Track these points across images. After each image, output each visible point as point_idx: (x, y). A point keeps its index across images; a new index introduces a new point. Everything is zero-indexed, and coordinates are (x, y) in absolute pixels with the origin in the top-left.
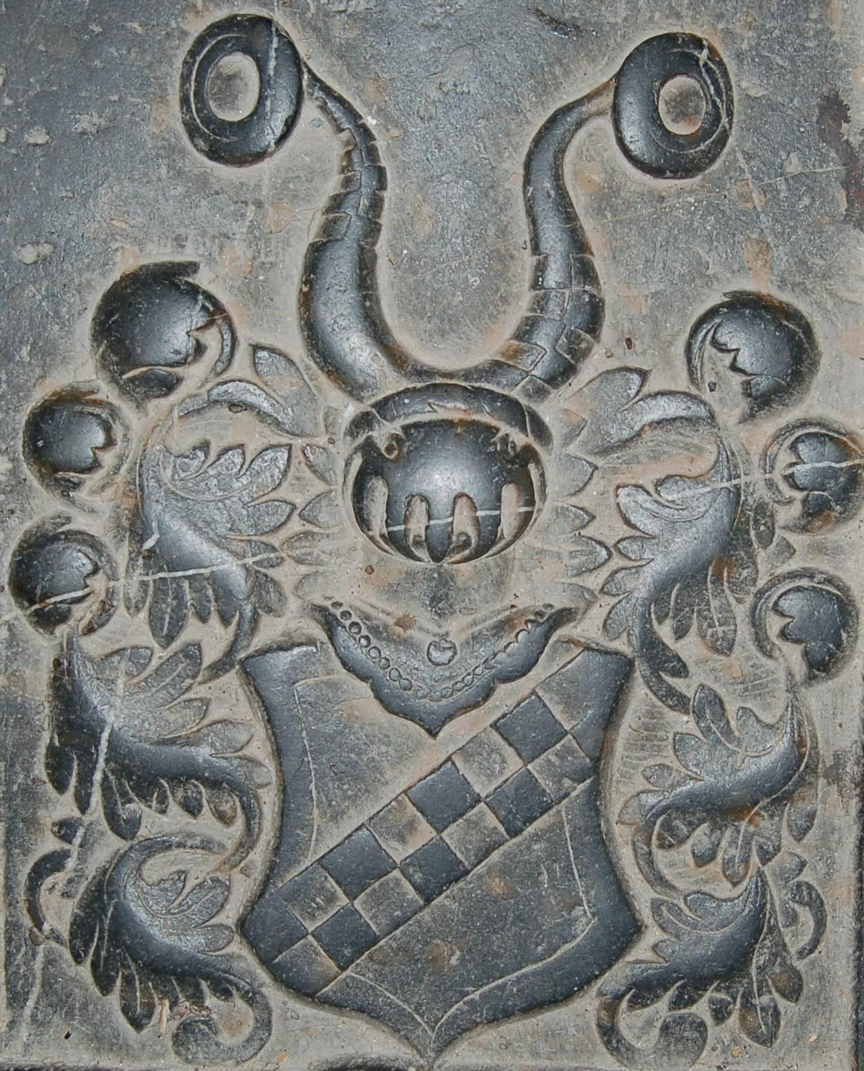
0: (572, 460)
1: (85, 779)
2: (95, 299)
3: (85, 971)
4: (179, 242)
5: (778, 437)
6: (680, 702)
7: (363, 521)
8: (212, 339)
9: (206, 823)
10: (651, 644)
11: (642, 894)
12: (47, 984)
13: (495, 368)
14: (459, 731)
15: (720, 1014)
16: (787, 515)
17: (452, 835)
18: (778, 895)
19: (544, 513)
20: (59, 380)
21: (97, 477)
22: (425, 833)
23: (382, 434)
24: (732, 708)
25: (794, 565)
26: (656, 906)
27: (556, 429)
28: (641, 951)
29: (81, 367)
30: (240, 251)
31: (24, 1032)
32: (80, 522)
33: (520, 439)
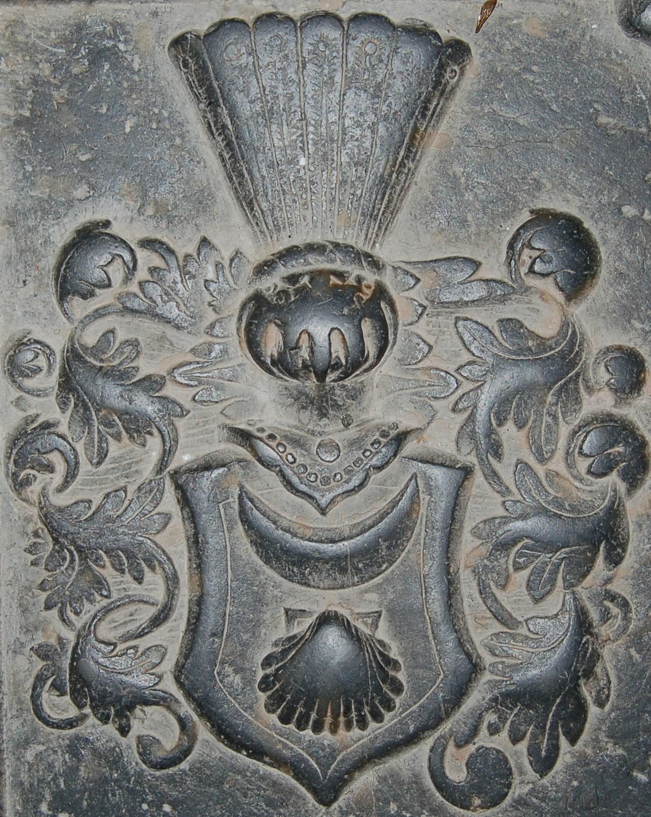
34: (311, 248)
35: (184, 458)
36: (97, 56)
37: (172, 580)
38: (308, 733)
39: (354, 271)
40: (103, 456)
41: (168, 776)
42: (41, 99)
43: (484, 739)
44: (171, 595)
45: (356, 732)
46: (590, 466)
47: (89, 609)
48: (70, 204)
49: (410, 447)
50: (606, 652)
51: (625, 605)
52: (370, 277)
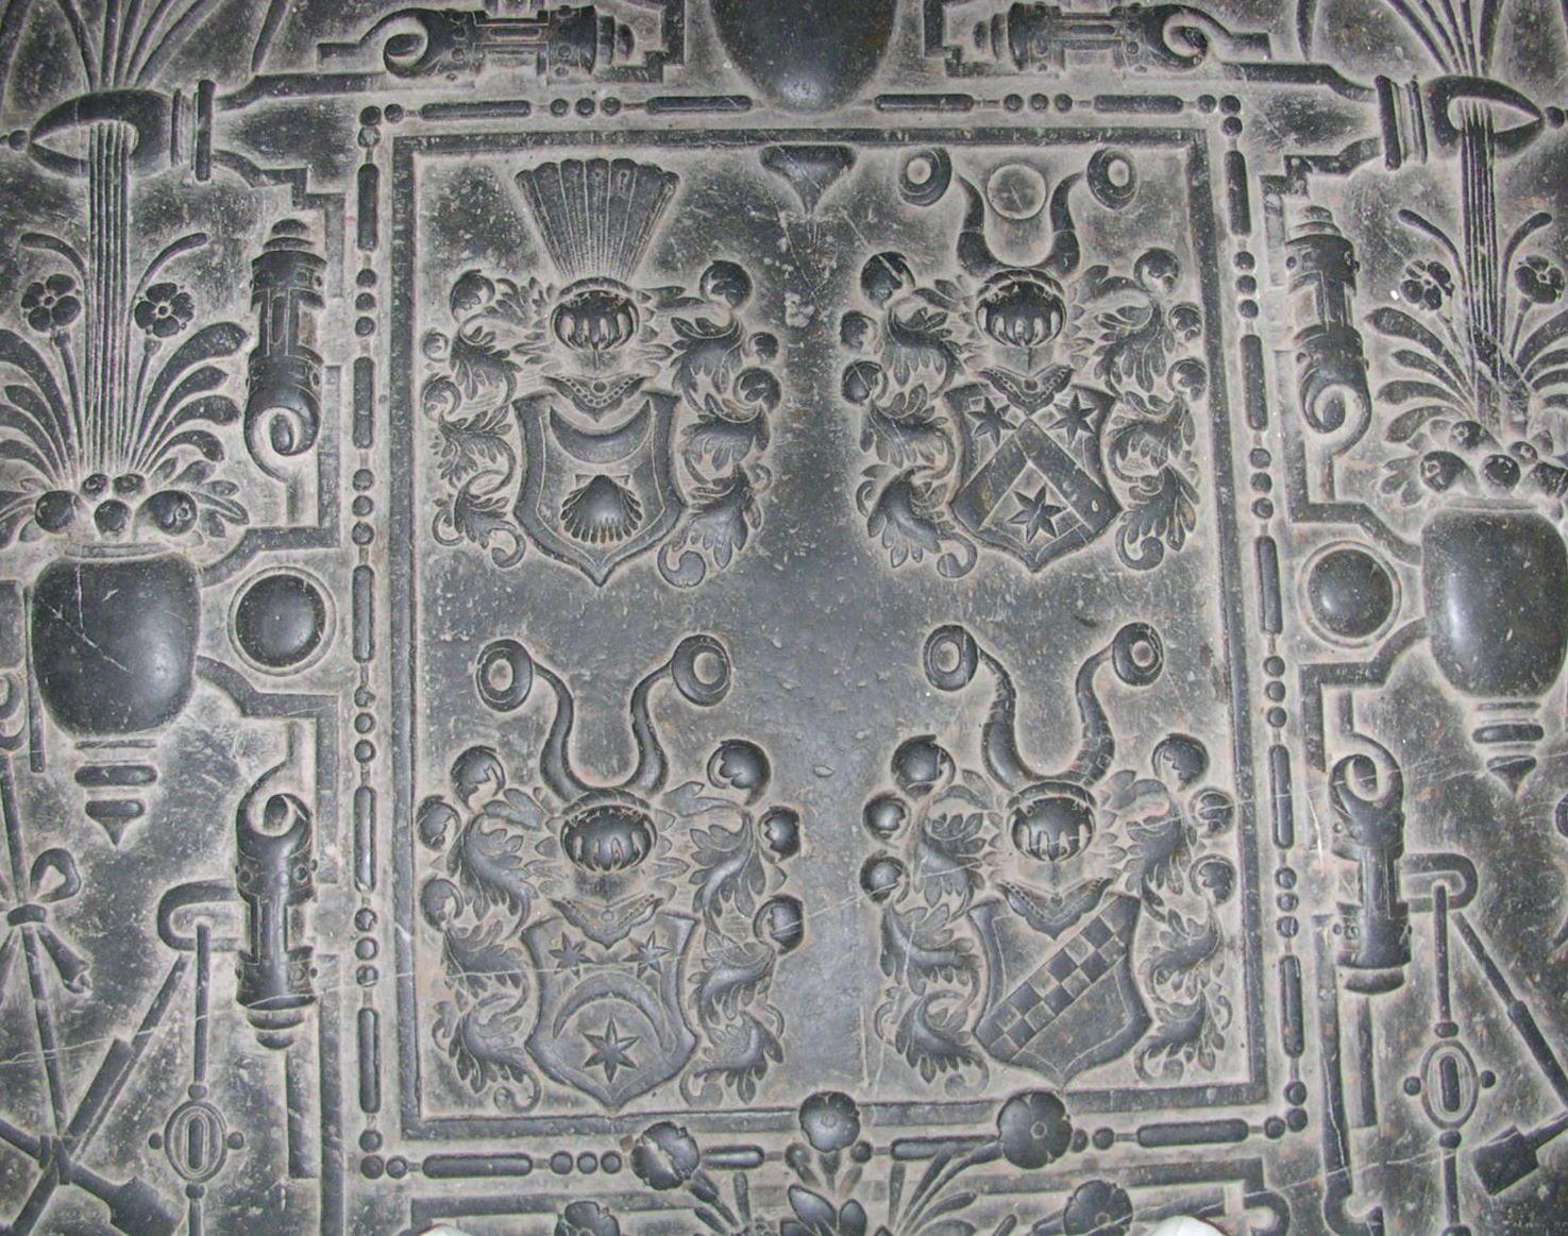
0: (1105, 813)
1: (900, 969)
2: (892, 753)
3: (903, 1057)
4: (927, 726)
5: (1195, 797)
6: (1161, 917)
7: (1018, 845)
8: (946, 767)
9: (955, 985)
10: (1147, 893)
11: (1151, 1006)
12: (886, 1067)
13: (1070, 774)
14: (1066, 936)
15: (1189, 1057)
16: (1202, 830)
17: (1066, 983)
18: (1210, 1002)
19: (1096, 838)
20: (877, 790)
21: (896, 834)
22: (1054, 984)
23: (1024, 806)
24: (1184, 919)
25: (1206, 853)
26: (1158, 1010)
27: (1098, 800)
28: (1153, 1031)
29: (888, 784)
30: (954, 728)
31: (876, 1087)
32: (891, 853)
33: (1084, 804)
34: (591, 280)
35: (517, 395)
36: (476, 185)
37: (512, 459)
38: (588, 543)
39: (614, 291)
40: (475, 391)
41: (517, 719)
42: (445, 207)
43: (689, 546)
44: (511, 468)
45: (616, 541)
46: (232, 520)
47: (466, 478)
48: (459, 262)
49: (646, 386)
50: (757, 498)
51: (768, 472)
52: (623, 295)
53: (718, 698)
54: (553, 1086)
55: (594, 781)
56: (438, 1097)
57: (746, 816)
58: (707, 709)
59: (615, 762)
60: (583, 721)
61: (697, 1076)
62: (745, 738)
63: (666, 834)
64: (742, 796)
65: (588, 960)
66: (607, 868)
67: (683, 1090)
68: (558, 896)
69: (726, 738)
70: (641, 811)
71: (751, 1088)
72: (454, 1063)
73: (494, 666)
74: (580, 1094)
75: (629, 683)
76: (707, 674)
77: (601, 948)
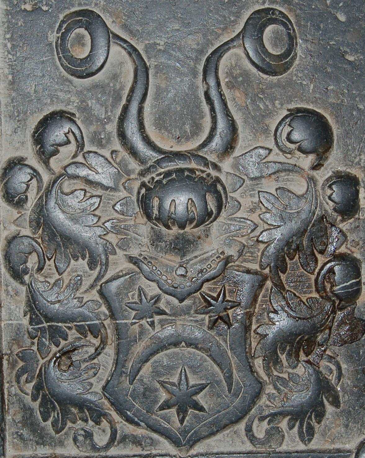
41: (95, 86)
53: (286, 67)
54: (130, 429)
55: (166, 145)
56: (21, 437)
57: (312, 180)
58: (275, 78)
59: (187, 128)
60: (158, 88)
61: (262, 419)
62: (310, 107)
63: (236, 195)
64: (307, 161)
65: (163, 313)
66: (182, 227)
67: (249, 429)
68: (134, 252)
69: (293, 106)
70: (214, 173)
71: (311, 432)
72: (36, 405)
73: (72, 35)
74: (155, 436)
75: (201, 52)
76: (275, 45)
77: (175, 301)
